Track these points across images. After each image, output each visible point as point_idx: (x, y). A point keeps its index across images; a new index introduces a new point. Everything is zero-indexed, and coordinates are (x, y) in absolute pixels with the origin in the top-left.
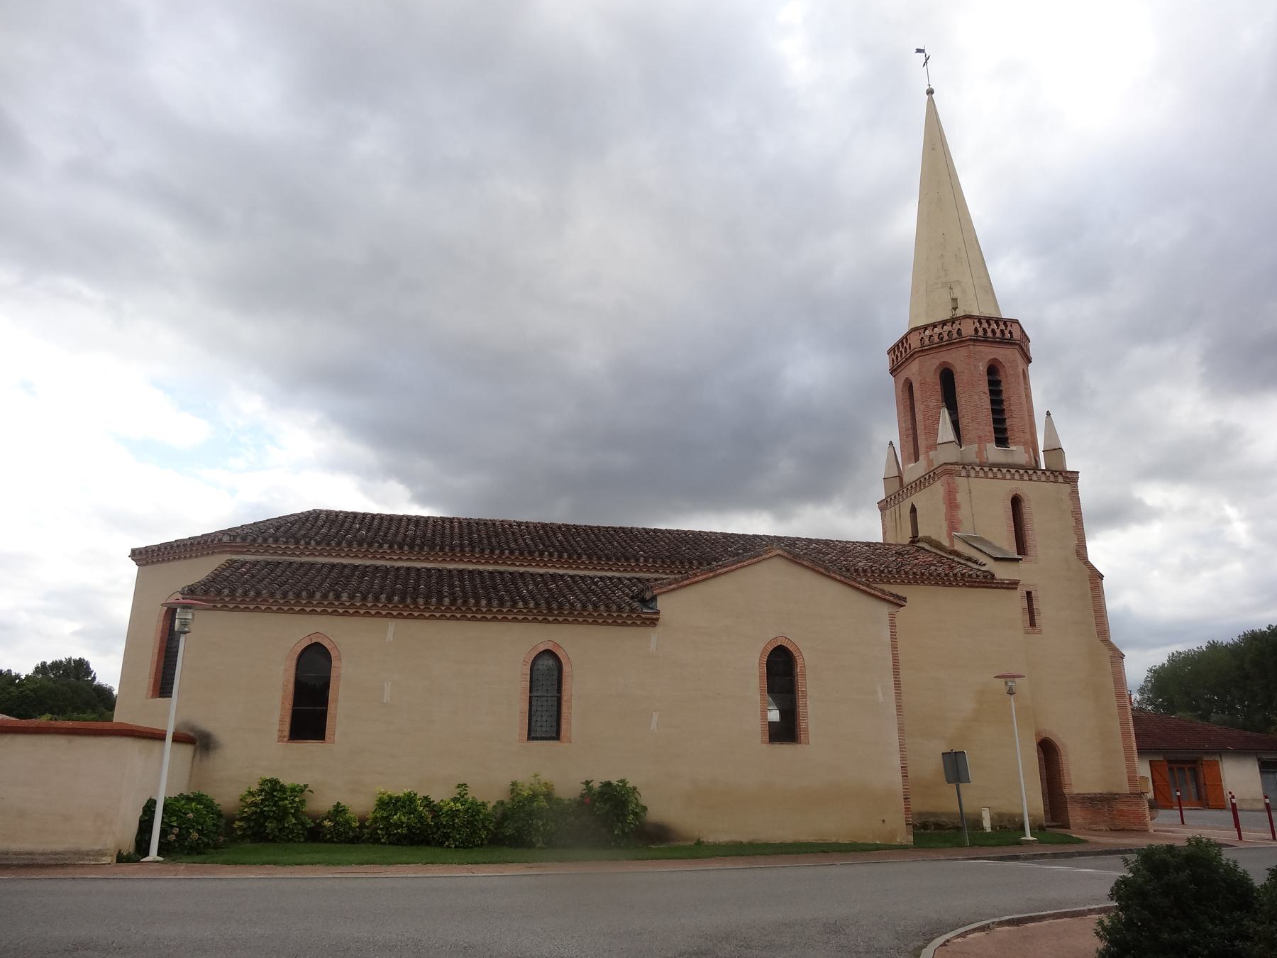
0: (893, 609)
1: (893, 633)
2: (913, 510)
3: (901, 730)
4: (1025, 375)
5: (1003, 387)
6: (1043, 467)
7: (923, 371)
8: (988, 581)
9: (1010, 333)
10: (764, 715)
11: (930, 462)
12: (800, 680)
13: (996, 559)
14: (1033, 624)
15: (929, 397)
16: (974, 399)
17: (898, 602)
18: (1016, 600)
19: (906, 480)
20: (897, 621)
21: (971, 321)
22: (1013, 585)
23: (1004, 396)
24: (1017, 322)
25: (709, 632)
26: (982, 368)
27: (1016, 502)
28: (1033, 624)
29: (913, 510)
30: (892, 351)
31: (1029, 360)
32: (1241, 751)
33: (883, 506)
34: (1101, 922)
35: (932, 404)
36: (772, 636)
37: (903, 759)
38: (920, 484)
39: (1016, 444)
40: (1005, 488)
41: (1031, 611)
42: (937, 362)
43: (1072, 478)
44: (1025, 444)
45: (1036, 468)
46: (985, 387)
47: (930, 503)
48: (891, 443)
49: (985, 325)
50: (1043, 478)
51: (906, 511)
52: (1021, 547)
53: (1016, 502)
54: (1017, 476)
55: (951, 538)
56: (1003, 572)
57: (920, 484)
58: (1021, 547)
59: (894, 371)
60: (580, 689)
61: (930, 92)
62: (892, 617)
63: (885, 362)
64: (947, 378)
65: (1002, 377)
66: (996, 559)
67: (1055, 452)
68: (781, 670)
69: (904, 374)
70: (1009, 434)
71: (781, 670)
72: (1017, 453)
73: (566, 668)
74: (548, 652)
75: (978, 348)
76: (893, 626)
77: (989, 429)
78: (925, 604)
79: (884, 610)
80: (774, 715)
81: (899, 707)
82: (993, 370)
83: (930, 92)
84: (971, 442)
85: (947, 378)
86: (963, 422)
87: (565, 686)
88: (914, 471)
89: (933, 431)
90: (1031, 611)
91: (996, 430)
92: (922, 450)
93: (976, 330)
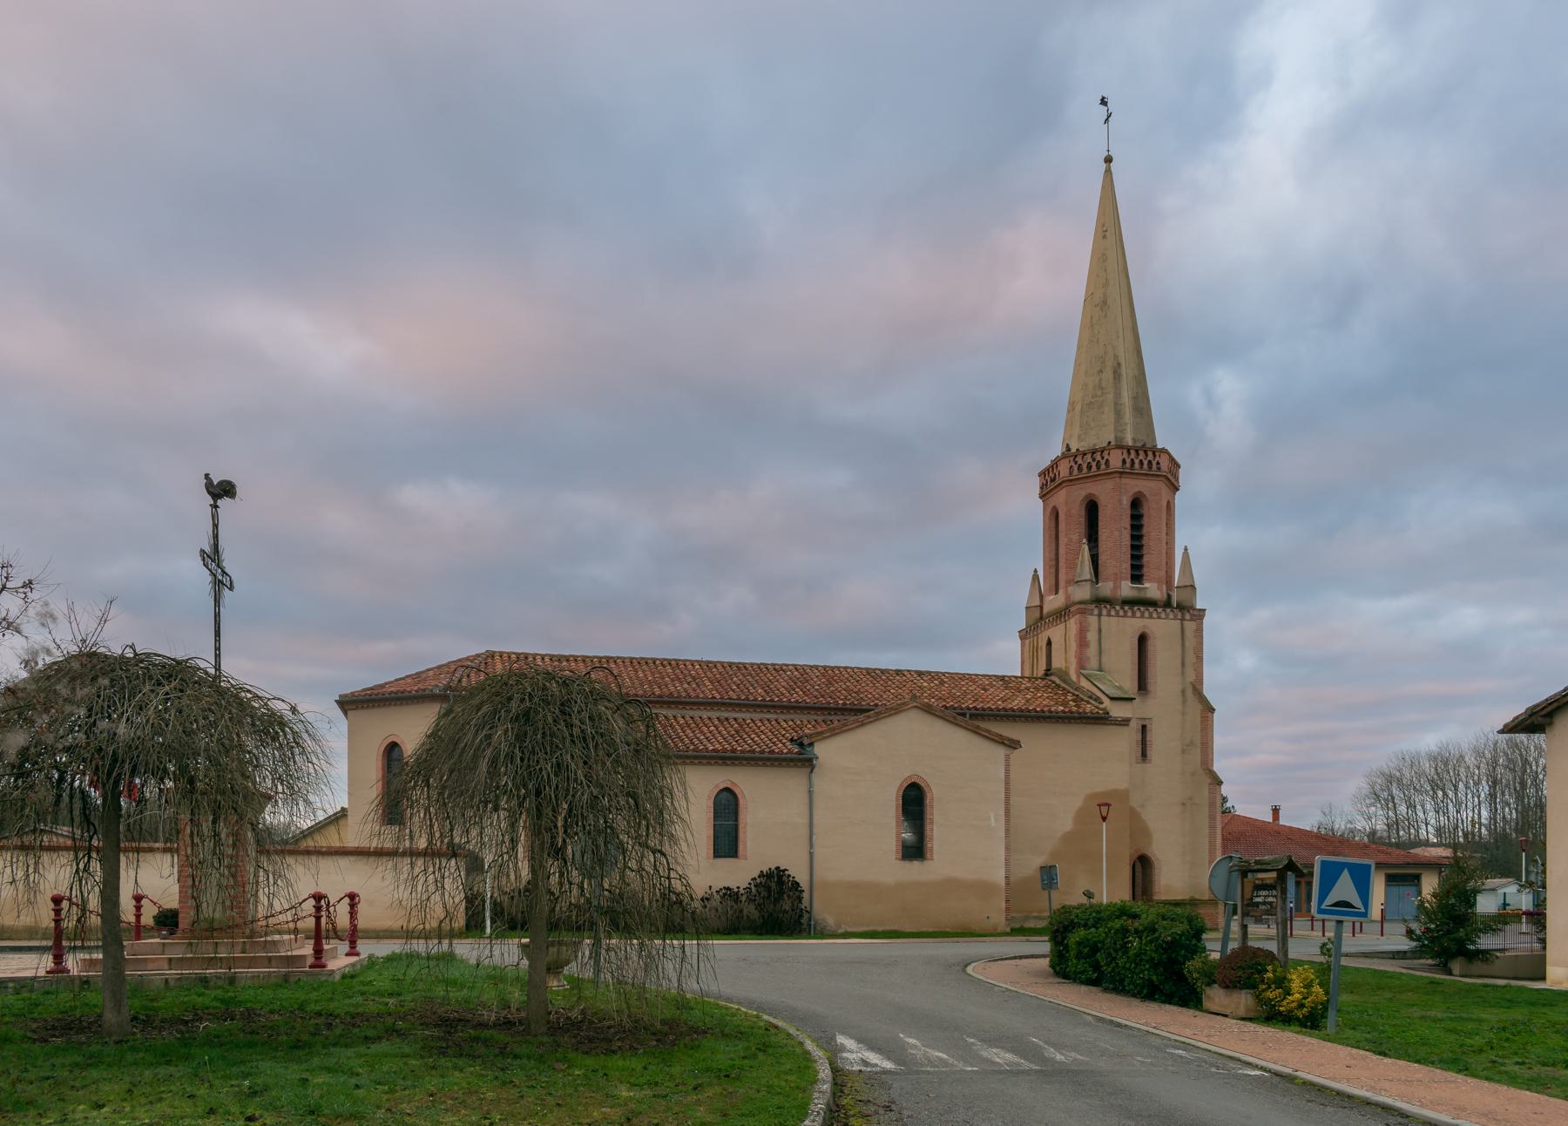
0: (1008, 751)
1: (1007, 771)
3: (1008, 848)
4: (1170, 507)
5: (1145, 521)
7: (1070, 500)
8: (1102, 719)
10: (898, 834)
11: (1068, 597)
12: (928, 810)
13: (1112, 699)
14: (1144, 755)
15: (1073, 532)
16: (1114, 534)
17: (1013, 745)
18: (1130, 735)
19: (1046, 610)
20: (1011, 762)
22: (1125, 722)
23: (1145, 531)
25: (859, 771)
26: (1126, 502)
27: (1143, 639)
28: (1144, 755)
29: (1049, 643)
30: (1042, 474)
33: (1024, 635)
35: (1075, 537)
36: (907, 774)
37: (1007, 871)
38: (1061, 614)
39: (1150, 581)
40: (1134, 624)
41: (1144, 743)
42: (1084, 493)
44: (1159, 581)
46: (1127, 522)
47: (1061, 636)
49: (1133, 455)
51: (1043, 644)
52: (1142, 685)
53: (1143, 639)
55: (1079, 674)
56: (1117, 711)
57: (1061, 614)
58: (1142, 685)
60: (890, 829)
61: (1108, 160)
62: (1007, 758)
65: (1144, 511)
66: (1112, 699)
68: (914, 802)
70: (1145, 570)
71: (914, 802)
72: (1152, 589)
73: (741, 802)
74: (727, 789)
75: (1124, 481)
76: (1007, 766)
77: (1126, 566)
78: (1037, 742)
79: (1000, 752)
80: (908, 836)
81: (1007, 831)
83: (1108, 160)
84: (1106, 580)
87: (741, 816)
88: (1054, 602)
89: (1072, 566)
90: (1144, 743)
91: (1133, 567)
92: (1062, 583)
93: (1124, 461)
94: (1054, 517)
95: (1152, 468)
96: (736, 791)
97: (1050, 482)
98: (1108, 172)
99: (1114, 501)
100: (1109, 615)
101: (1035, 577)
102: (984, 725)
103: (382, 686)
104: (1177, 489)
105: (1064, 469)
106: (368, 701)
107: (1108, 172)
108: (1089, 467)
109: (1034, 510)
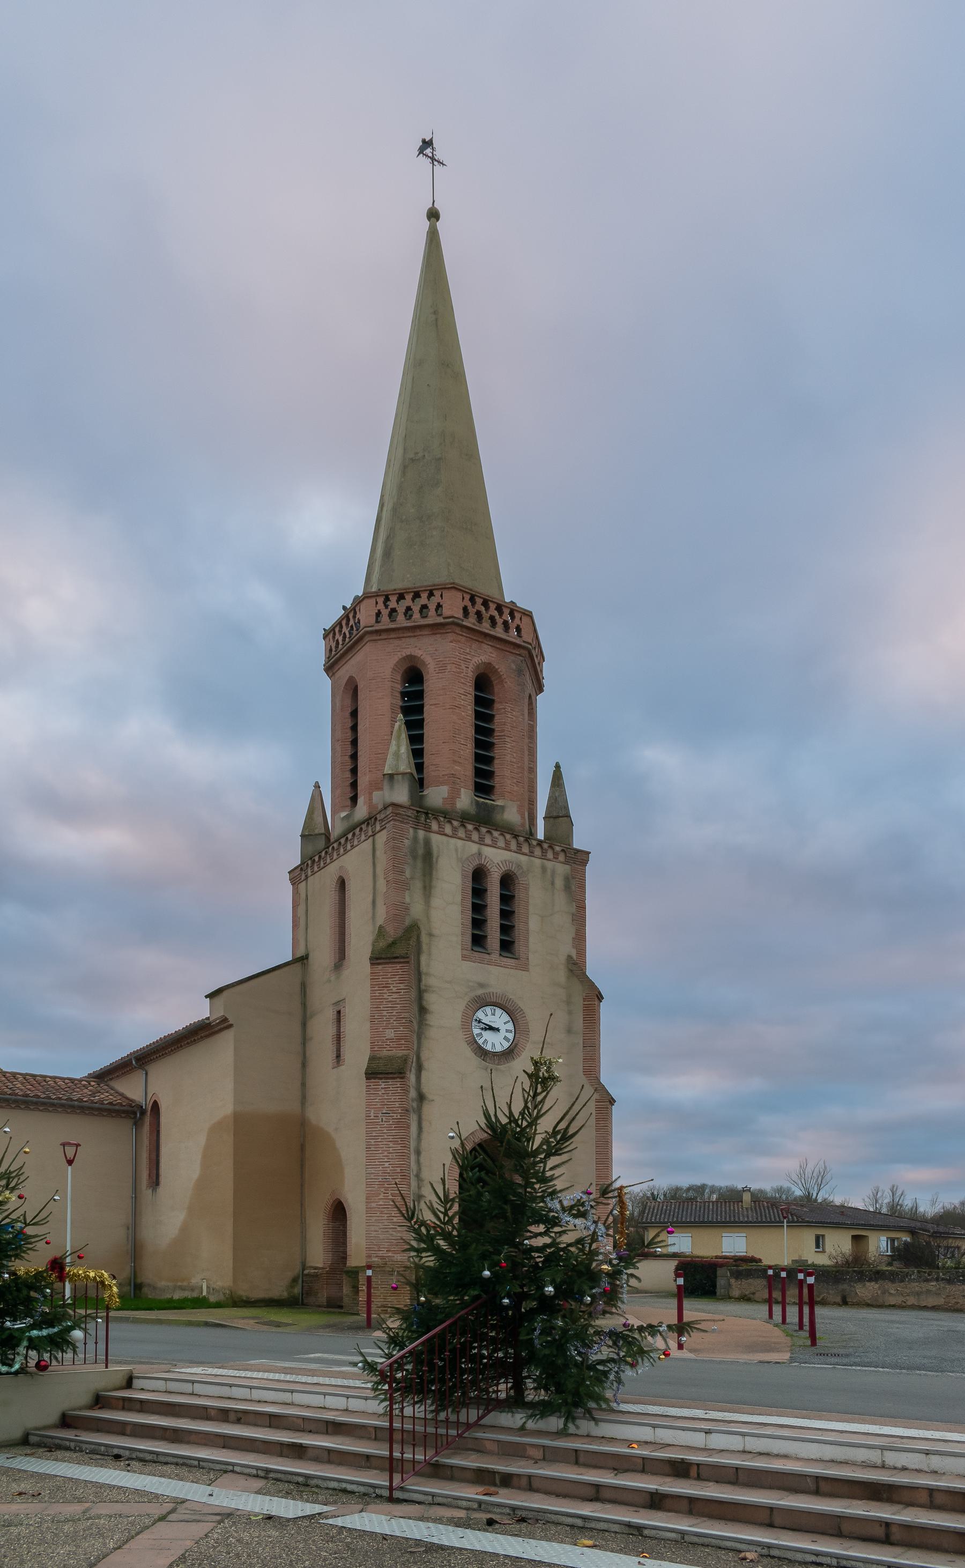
2: (342, 884)
6: (540, 835)
7: (379, 666)
9: (518, 629)
21: (459, 595)
24: (528, 614)
30: (328, 634)
31: (540, 688)
32: (490, 1278)
34: (577, 1427)
43: (579, 859)
45: (531, 834)
48: (317, 786)
50: (538, 851)
54: (501, 843)
59: (330, 668)
63: (318, 651)
64: (413, 677)
67: (559, 814)
69: (346, 670)
82: (483, 684)
83: (433, 215)
85: (413, 677)
86: (429, 745)
91: (479, 773)
98: (433, 239)
107: (433, 239)
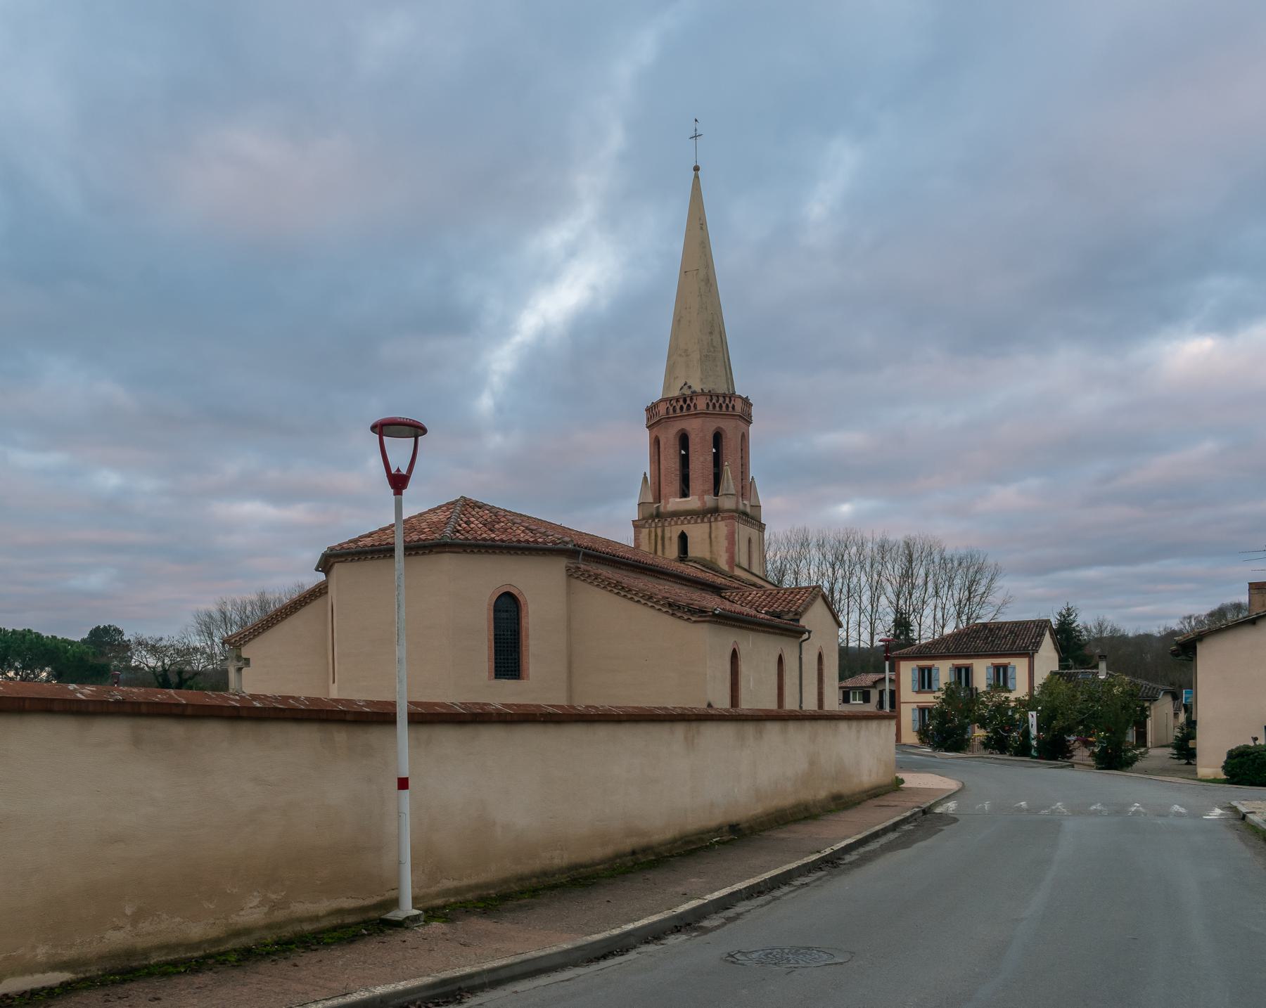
4: (744, 438)
7: (669, 436)
26: (710, 438)
30: (648, 410)
61: (696, 169)
83: (696, 169)
94: (656, 443)
95: (730, 410)
96: (515, 592)
97: (657, 417)
98: (697, 177)
99: (700, 431)
100: (670, 525)
101: (645, 478)
102: (66, 976)
103: (355, 541)
104: (749, 422)
105: (662, 409)
106: (372, 552)
107: (697, 177)
108: (682, 408)
109: (644, 437)
